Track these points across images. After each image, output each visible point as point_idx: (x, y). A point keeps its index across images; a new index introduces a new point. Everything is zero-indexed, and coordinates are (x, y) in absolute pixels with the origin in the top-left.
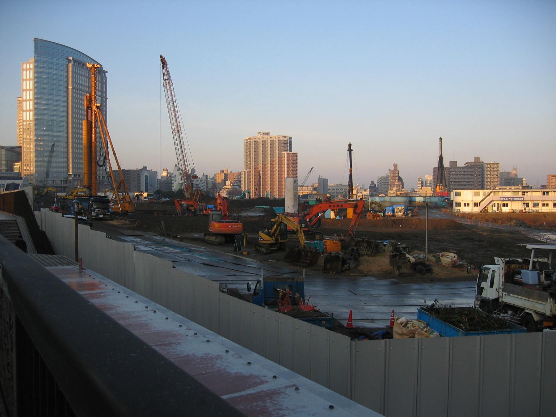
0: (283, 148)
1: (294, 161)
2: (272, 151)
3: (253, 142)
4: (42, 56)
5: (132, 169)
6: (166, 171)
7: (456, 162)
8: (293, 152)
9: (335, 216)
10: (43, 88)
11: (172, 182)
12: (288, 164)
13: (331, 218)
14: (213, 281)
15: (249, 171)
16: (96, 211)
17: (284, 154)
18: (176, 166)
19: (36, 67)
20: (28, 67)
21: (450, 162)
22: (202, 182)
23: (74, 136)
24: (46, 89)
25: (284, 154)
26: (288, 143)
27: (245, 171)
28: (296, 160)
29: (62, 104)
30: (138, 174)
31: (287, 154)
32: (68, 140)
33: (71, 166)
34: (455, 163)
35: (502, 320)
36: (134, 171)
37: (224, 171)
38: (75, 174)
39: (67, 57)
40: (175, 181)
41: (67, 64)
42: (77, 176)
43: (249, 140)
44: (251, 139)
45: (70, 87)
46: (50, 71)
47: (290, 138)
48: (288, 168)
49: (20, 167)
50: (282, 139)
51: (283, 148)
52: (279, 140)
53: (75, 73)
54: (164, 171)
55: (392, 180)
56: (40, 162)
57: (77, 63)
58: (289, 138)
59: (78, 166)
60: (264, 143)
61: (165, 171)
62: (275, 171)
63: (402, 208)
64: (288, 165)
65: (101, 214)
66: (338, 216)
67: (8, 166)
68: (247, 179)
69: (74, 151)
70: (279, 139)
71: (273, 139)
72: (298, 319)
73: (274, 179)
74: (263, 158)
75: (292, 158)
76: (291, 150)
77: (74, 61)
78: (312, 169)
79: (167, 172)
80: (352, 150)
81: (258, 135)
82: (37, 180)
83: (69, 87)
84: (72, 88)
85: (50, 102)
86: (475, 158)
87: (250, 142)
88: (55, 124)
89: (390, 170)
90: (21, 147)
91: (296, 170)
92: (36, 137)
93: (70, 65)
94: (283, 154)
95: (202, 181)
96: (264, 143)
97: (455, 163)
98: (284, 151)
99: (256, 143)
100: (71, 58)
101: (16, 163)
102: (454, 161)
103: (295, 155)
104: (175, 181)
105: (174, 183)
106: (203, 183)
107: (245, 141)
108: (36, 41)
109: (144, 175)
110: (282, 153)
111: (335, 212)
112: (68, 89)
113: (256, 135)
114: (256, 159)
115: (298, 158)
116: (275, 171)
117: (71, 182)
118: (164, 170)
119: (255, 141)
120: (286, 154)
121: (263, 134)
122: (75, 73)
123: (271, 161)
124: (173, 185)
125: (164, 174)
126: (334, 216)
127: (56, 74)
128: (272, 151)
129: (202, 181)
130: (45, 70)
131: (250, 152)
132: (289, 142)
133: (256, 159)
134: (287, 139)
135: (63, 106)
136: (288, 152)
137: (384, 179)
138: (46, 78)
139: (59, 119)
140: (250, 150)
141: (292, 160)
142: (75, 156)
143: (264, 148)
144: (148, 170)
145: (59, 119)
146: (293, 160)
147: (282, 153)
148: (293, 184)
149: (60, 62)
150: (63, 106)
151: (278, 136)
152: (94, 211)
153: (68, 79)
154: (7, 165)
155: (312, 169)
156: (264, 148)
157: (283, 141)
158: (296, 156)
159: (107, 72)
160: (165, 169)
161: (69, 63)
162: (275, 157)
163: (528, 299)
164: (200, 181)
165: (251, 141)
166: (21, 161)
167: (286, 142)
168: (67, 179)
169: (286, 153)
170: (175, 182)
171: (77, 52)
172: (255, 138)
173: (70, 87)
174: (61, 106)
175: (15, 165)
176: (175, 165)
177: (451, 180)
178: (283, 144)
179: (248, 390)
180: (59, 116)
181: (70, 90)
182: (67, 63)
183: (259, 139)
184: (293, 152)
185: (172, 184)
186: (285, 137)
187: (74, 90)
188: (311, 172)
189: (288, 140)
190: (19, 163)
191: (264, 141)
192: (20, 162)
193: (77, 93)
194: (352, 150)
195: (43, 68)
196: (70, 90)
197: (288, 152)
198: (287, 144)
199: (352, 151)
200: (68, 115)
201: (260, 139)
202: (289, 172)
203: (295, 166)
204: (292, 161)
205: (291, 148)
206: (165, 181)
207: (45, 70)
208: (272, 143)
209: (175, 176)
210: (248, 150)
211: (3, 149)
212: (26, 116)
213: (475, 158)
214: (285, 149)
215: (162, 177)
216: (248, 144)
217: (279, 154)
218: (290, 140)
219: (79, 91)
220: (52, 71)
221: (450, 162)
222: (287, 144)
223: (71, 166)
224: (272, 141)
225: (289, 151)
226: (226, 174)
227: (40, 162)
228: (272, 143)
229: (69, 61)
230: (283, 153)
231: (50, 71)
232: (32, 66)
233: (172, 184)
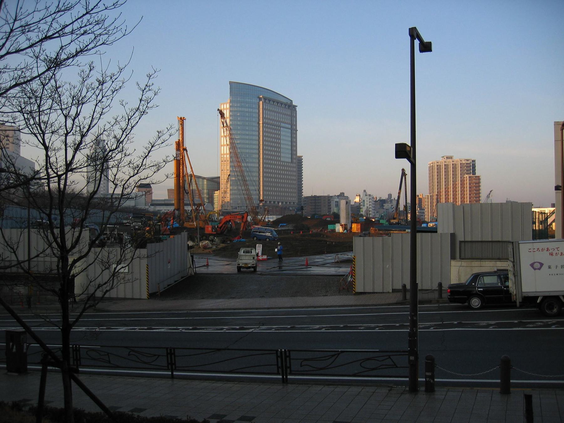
0: (465, 171)
1: (477, 184)
2: (455, 175)
3: (436, 166)
4: (236, 97)
5: (323, 195)
6: (359, 197)
8: (477, 175)
9: (343, 230)
10: (238, 125)
11: (361, 207)
12: (470, 188)
13: (340, 232)
16: (133, 224)
17: (467, 177)
19: (230, 107)
20: (225, 107)
22: (392, 207)
23: (265, 166)
24: (240, 125)
25: (467, 177)
26: (470, 166)
27: (428, 196)
28: (479, 183)
29: (254, 138)
30: (329, 200)
31: (469, 177)
32: (259, 170)
33: (261, 193)
36: (324, 197)
37: (419, 196)
38: (282, 201)
39: (258, 96)
40: (364, 206)
41: (258, 103)
42: (292, 203)
43: (431, 165)
44: (441, 163)
45: (261, 122)
46: (243, 109)
47: (474, 161)
48: (471, 191)
49: (219, 195)
50: (464, 162)
51: (465, 171)
52: (461, 164)
53: (266, 109)
54: (356, 197)
56: (235, 190)
57: (267, 100)
58: (471, 161)
59: (284, 195)
60: (446, 166)
61: (357, 197)
62: (458, 195)
63: (433, 225)
64: (470, 189)
65: (137, 226)
66: (345, 231)
67: (209, 194)
68: (430, 203)
69: (265, 179)
70: (461, 162)
71: (455, 163)
72: (229, 298)
73: (457, 202)
74: (445, 182)
75: (474, 181)
76: (474, 173)
77: (264, 99)
78: (491, 192)
79: (360, 198)
80: (407, 175)
81: (442, 159)
82: (232, 206)
83: (260, 123)
84: (262, 123)
85: (243, 137)
87: (433, 166)
88: (247, 156)
90: (219, 177)
91: (479, 193)
92: (231, 168)
93: (261, 102)
94: (465, 177)
95: (393, 205)
96: (446, 166)
98: (467, 174)
99: (439, 167)
100: (261, 96)
101: (216, 192)
103: (478, 178)
104: (364, 206)
105: (362, 208)
106: (394, 207)
107: (429, 166)
108: (231, 83)
109: (334, 200)
110: (464, 176)
111: (343, 227)
112: (259, 124)
113: (441, 160)
114: (439, 183)
115: (482, 181)
116: (458, 195)
117: (262, 208)
118: (357, 195)
119: (437, 166)
120: (468, 178)
121: (447, 158)
122: (266, 109)
123: (453, 185)
124: (361, 210)
125: (357, 199)
126: (342, 230)
127: (248, 112)
128: (455, 175)
129: (393, 205)
130: (239, 109)
131: (433, 176)
132: (471, 164)
133: (439, 183)
134: (469, 162)
135: (255, 140)
136: (471, 175)
138: (239, 116)
139: (252, 151)
140: (433, 174)
141: (475, 183)
142: (269, 185)
143: (447, 172)
144: (345, 195)
145: (252, 151)
146: (476, 184)
147: (464, 176)
148: (345, 205)
149: (251, 101)
150: (255, 140)
151: (460, 159)
152: (132, 224)
153: (259, 116)
154: (208, 194)
155: (491, 192)
156: (447, 172)
157: (465, 164)
158: (479, 179)
159: (297, 106)
160: (358, 195)
161: (260, 101)
162: (457, 181)
164: (390, 206)
165: (434, 165)
166: (220, 190)
167: (469, 165)
168: (259, 205)
169: (468, 176)
170: (364, 207)
171: (270, 91)
172: (461, 161)
173: (261, 122)
174: (253, 140)
175: (214, 193)
176: (364, 190)
178: (465, 167)
180: (251, 149)
181: (261, 125)
182: (258, 101)
183: (449, 163)
184: (477, 175)
185: (361, 208)
186: (468, 160)
187: (265, 125)
188: (490, 194)
189: (470, 163)
190: (218, 192)
191: (447, 164)
192: (219, 190)
193: (268, 128)
194: (407, 175)
195: (237, 107)
196: (261, 125)
197: (471, 175)
198: (471, 167)
199: (406, 176)
200: (259, 147)
201: (450, 163)
202: (472, 195)
203: (478, 188)
204: (474, 184)
206: (357, 206)
207: (239, 109)
208: (454, 167)
209: (364, 201)
210: (431, 175)
211: (200, 179)
212: (224, 150)
214: (467, 172)
215: (355, 202)
216: (431, 168)
217: (461, 178)
218: (474, 163)
219: (273, 127)
220: (241, 109)
222: (471, 167)
223: (261, 193)
224: (454, 165)
225: (472, 174)
226: (421, 198)
227: (235, 190)
228: (454, 167)
229: (260, 99)
230: (465, 176)
231: (243, 109)
232: (228, 106)
233: (361, 208)
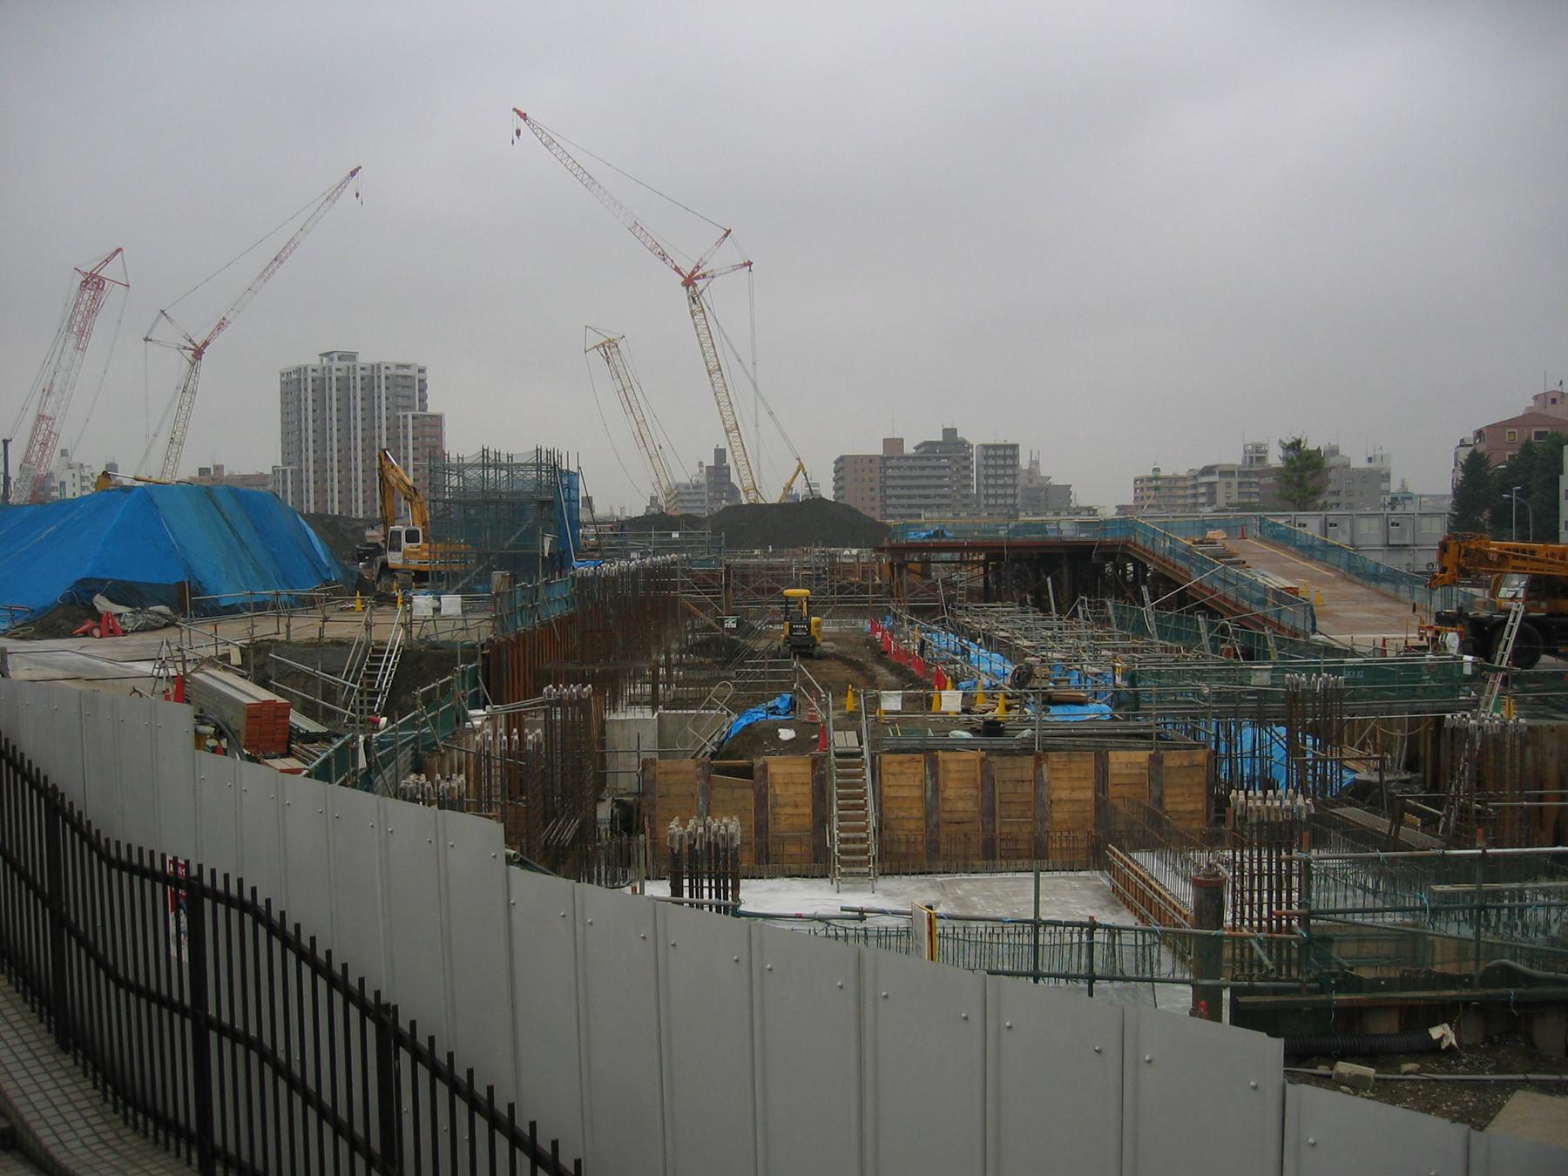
7: (902, 440)
8: (430, 411)
14: (1010, 978)
15: (296, 468)
17: (405, 417)
18: (62, 455)
21: (884, 440)
34: (899, 443)
35: (631, 808)
43: (294, 376)
47: (422, 371)
55: (711, 494)
76: (424, 407)
86: (945, 431)
87: (299, 380)
89: (701, 464)
97: (899, 443)
102: (896, 437)
137: (687, 491)
163: (1444, 854)
165: (302, 377)
177: (889, 492)
179: (68, 1061)
205: (422, 400)
209: (63, 484)
213: (945, 431)
218: (421, 376)
221: (884, 440)
